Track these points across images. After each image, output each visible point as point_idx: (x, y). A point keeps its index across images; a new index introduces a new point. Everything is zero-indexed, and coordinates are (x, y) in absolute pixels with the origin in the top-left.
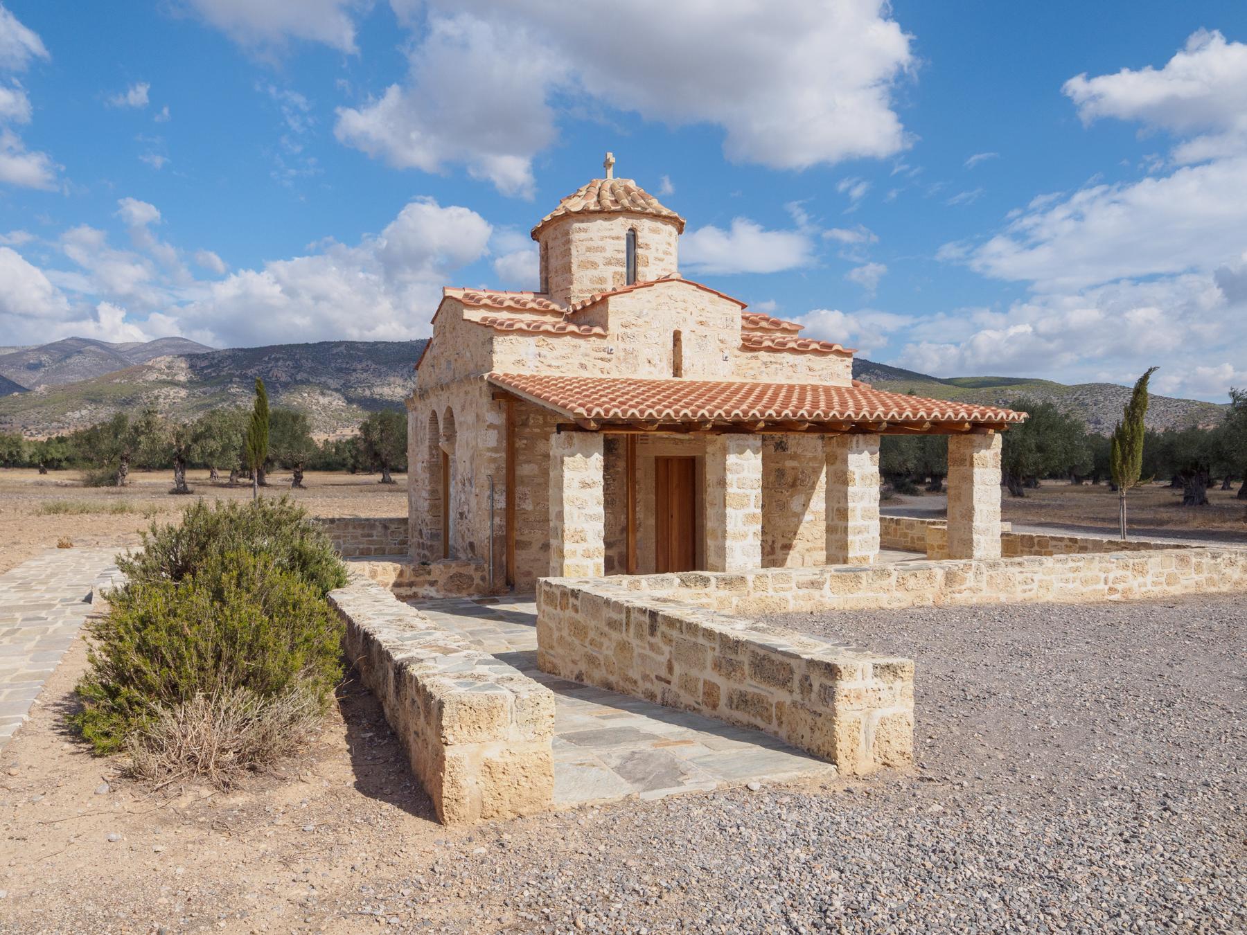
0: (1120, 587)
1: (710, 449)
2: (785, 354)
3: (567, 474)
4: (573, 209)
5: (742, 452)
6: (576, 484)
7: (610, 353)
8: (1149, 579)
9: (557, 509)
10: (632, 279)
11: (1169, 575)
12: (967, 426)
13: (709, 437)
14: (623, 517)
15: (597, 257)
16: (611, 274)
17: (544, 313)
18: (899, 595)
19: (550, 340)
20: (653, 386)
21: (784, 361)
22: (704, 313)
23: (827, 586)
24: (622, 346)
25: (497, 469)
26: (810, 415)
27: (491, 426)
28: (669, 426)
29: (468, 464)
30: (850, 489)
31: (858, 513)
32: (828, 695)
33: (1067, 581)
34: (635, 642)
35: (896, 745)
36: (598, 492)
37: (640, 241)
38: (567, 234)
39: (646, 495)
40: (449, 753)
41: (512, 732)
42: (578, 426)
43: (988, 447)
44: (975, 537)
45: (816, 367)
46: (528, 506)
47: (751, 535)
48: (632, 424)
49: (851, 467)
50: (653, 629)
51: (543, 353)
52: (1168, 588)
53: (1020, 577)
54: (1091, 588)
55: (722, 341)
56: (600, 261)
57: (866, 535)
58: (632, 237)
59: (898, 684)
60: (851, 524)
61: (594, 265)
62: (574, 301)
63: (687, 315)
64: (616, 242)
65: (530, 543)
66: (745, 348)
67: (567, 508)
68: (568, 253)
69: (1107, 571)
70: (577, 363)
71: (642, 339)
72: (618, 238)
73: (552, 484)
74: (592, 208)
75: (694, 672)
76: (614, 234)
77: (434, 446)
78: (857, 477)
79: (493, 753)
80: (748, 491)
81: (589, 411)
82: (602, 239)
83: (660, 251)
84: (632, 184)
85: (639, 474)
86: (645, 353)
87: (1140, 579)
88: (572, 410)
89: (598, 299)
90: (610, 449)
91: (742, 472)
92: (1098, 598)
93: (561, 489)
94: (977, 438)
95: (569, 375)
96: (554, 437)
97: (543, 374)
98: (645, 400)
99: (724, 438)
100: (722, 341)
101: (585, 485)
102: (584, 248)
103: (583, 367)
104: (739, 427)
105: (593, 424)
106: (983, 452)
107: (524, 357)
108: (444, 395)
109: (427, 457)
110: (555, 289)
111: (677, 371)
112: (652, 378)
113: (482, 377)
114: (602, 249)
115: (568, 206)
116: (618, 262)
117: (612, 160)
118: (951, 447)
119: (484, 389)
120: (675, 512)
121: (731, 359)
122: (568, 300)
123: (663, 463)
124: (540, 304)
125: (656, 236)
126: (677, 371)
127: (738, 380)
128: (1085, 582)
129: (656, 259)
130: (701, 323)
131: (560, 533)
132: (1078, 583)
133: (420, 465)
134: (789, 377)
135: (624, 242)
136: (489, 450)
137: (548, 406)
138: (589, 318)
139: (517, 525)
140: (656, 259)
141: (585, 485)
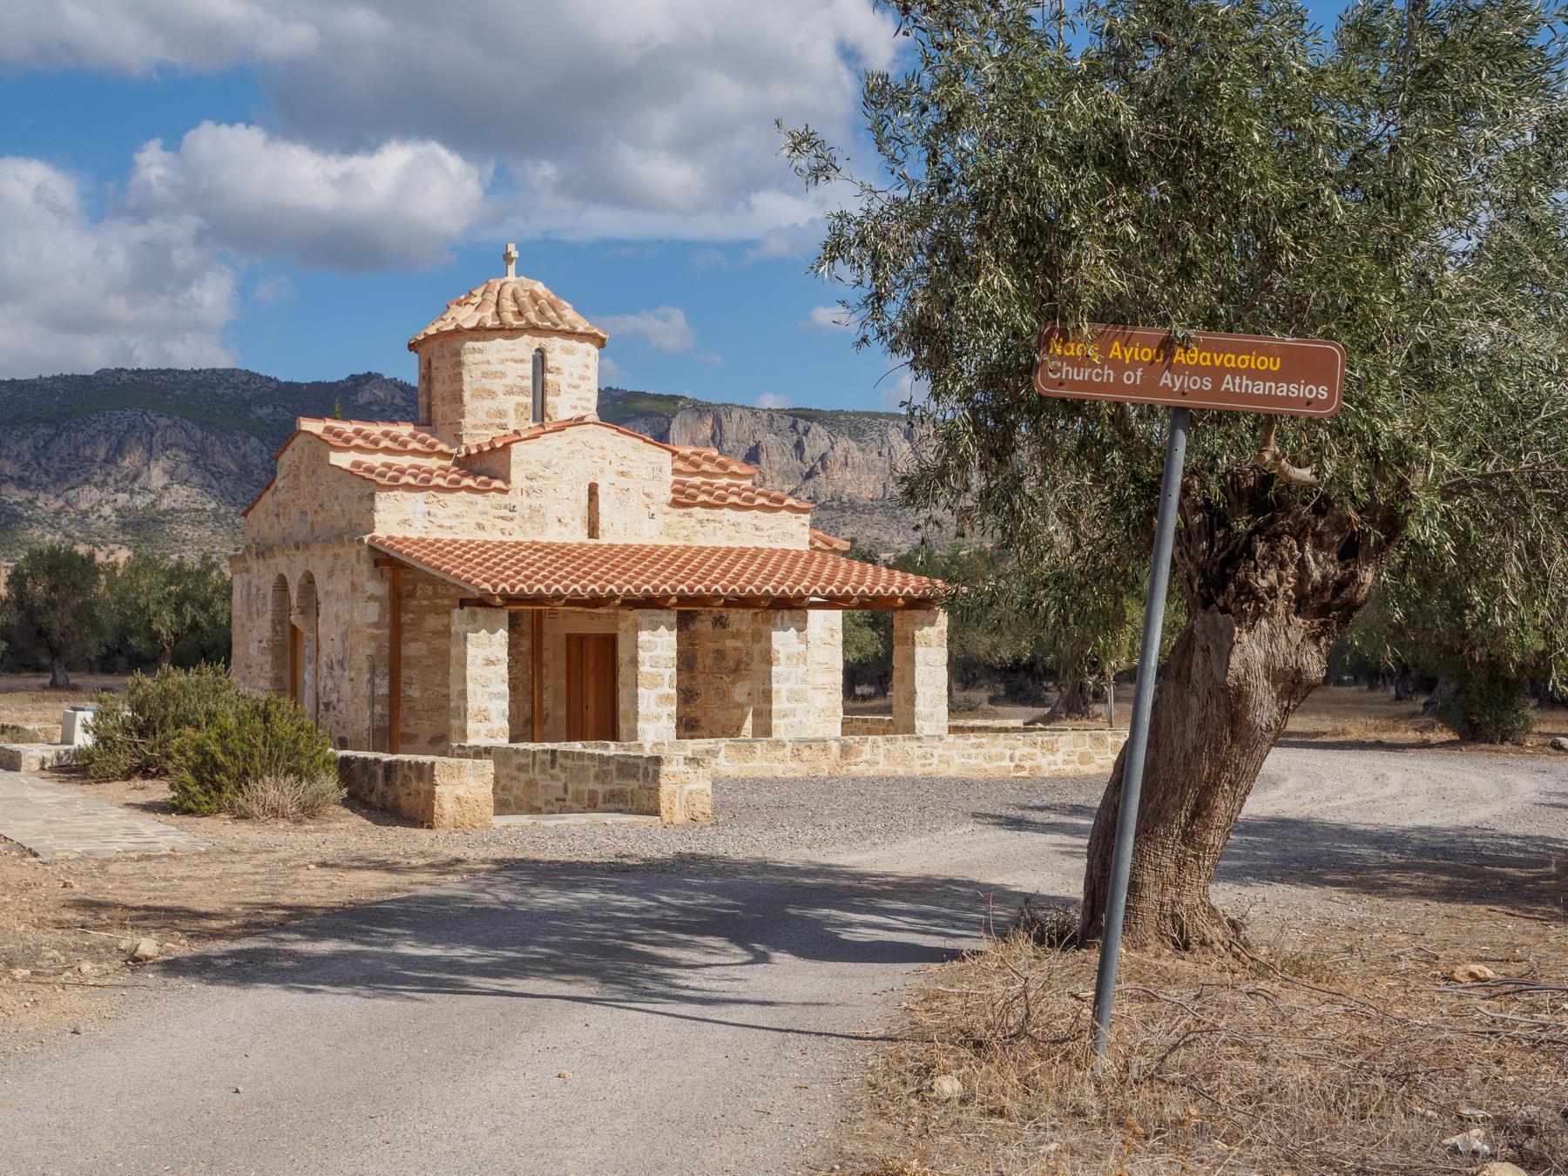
0: (1027, 764)
1: (622, 625)
2: (725, 510)
3: (471, 651)
4: (467, 325)
5: (655, 629)
6: (480, 661)
7: (513, 510)
8: (1060, 757)
9: (459, 688)
10: (540, 411)
11: (1082, 755)
12: (900, 601)
13: (621, 612)
14: (527, 707)
15: (496, 385)
16: (513, 408)
17: (428, 455)
18: (794, 765)
19: (441, 496)
20: (562, 552)
21: (724, 519)
22: (626, 462)
23: (722, 755)
24: (527, 502)
25: (379, 648)
26: (725, 590)
27: (372, 598)
28: (575, 601)
29: (338, 642)
30: (774, 669)
31: (784, 695)
32: (657, 774)
33: (969, 756)
34: (539, 777)
35: (699, 808)
36: (503, 669)
37: (549, 364)
38: (458, 354)
39: (555, 678)
40: (438, 789)
41: (471, 781)
42: (483, 602)
43: (932, 624)
44: (917, 723)
45: (764, 526)
46: (414, 692)
47: (665, 717)
48: (538, 599)
49: (775, 646)
50: (553, 763)
51: (433, 511)
52: (1081, 768)
53: (919, 752)
54: (995, 764)
55: (648, 495)
56: (500, 390)
57: (792, 719)
58: (540, 359)
59: (700, 770)
60: (774, 707)
61: (491, 394)
62: (466, 440)
63: (604, 464)
64: (519, 366)
65: (417, 736)
66: (675, 504)
67: (470, 686)
68: (458, 378)
69: (1013, 748)
70: (473, 523)
71: (551, 493)
72: (522, 361)
73: (453, 662)
74: (489, 324)
75: (582, 787)
76: (517, 355)
77: (281, 618)
78: (781, 655)
79: (461, 791)
80: (662, 670)
81: (495, 586)
82: (502, 362)
83: (575, 376)
84: (540, 288)
85: (547, 655)
86: (555, 510)
87: (1050, 758)
88: (477, 585)
89: (499, 445)
90: (513, 627)
91: (656, 650)
92: (1004, 773)
93: (464, 666)
94: (919, 614)
95: (463, 538)
96: (456, 612)
97: (432, 537)
98: (552, 573)
99: (635, 614)
100: (648, 495)
101: (489, 662)
102: (479, 373)
103: (480, 527)
104: (651, 603)
105: (498, 600)
106: (926, 629)
107: (411, 516)
108: (300, 557)
109: (268, 634)
110: (440, 421)
111: (593, 531)
112: (559, 540)
113: (361, 541)
114: (502, 375)
115: (460, 319)
116: (522, 391)
117: (515, 254)
118: (896, 623)
119: (364, 553)
120: (591, 702)
121: (659, 517)
122: (458, 439)
123: (576, 643)
124: (422, 441)
125: (570, 358)
126: (593, 531)
127: (666, 542)
128: (989, 758)
129: (570, 386)
130: (623, 474)
131: (462, 713)
132: (980, 760)
133: (253, 648)
134: (730, 538)
135: (530, 366)
136: (369, 625)
137: (449, 579)
138: (485, 467)
139: (402, 715)
140: (570, 386)
141: (489, 662)
